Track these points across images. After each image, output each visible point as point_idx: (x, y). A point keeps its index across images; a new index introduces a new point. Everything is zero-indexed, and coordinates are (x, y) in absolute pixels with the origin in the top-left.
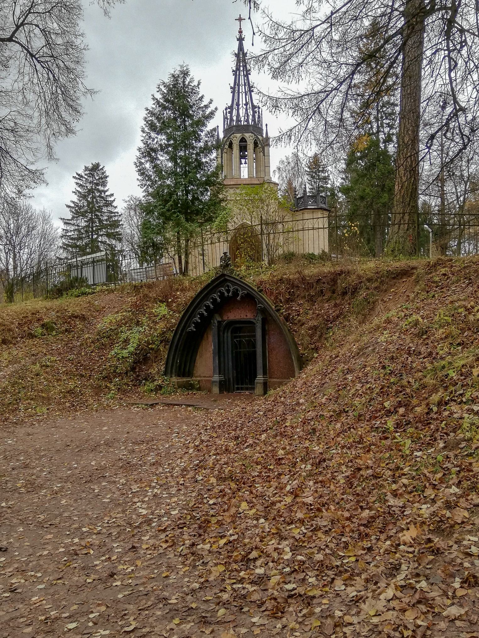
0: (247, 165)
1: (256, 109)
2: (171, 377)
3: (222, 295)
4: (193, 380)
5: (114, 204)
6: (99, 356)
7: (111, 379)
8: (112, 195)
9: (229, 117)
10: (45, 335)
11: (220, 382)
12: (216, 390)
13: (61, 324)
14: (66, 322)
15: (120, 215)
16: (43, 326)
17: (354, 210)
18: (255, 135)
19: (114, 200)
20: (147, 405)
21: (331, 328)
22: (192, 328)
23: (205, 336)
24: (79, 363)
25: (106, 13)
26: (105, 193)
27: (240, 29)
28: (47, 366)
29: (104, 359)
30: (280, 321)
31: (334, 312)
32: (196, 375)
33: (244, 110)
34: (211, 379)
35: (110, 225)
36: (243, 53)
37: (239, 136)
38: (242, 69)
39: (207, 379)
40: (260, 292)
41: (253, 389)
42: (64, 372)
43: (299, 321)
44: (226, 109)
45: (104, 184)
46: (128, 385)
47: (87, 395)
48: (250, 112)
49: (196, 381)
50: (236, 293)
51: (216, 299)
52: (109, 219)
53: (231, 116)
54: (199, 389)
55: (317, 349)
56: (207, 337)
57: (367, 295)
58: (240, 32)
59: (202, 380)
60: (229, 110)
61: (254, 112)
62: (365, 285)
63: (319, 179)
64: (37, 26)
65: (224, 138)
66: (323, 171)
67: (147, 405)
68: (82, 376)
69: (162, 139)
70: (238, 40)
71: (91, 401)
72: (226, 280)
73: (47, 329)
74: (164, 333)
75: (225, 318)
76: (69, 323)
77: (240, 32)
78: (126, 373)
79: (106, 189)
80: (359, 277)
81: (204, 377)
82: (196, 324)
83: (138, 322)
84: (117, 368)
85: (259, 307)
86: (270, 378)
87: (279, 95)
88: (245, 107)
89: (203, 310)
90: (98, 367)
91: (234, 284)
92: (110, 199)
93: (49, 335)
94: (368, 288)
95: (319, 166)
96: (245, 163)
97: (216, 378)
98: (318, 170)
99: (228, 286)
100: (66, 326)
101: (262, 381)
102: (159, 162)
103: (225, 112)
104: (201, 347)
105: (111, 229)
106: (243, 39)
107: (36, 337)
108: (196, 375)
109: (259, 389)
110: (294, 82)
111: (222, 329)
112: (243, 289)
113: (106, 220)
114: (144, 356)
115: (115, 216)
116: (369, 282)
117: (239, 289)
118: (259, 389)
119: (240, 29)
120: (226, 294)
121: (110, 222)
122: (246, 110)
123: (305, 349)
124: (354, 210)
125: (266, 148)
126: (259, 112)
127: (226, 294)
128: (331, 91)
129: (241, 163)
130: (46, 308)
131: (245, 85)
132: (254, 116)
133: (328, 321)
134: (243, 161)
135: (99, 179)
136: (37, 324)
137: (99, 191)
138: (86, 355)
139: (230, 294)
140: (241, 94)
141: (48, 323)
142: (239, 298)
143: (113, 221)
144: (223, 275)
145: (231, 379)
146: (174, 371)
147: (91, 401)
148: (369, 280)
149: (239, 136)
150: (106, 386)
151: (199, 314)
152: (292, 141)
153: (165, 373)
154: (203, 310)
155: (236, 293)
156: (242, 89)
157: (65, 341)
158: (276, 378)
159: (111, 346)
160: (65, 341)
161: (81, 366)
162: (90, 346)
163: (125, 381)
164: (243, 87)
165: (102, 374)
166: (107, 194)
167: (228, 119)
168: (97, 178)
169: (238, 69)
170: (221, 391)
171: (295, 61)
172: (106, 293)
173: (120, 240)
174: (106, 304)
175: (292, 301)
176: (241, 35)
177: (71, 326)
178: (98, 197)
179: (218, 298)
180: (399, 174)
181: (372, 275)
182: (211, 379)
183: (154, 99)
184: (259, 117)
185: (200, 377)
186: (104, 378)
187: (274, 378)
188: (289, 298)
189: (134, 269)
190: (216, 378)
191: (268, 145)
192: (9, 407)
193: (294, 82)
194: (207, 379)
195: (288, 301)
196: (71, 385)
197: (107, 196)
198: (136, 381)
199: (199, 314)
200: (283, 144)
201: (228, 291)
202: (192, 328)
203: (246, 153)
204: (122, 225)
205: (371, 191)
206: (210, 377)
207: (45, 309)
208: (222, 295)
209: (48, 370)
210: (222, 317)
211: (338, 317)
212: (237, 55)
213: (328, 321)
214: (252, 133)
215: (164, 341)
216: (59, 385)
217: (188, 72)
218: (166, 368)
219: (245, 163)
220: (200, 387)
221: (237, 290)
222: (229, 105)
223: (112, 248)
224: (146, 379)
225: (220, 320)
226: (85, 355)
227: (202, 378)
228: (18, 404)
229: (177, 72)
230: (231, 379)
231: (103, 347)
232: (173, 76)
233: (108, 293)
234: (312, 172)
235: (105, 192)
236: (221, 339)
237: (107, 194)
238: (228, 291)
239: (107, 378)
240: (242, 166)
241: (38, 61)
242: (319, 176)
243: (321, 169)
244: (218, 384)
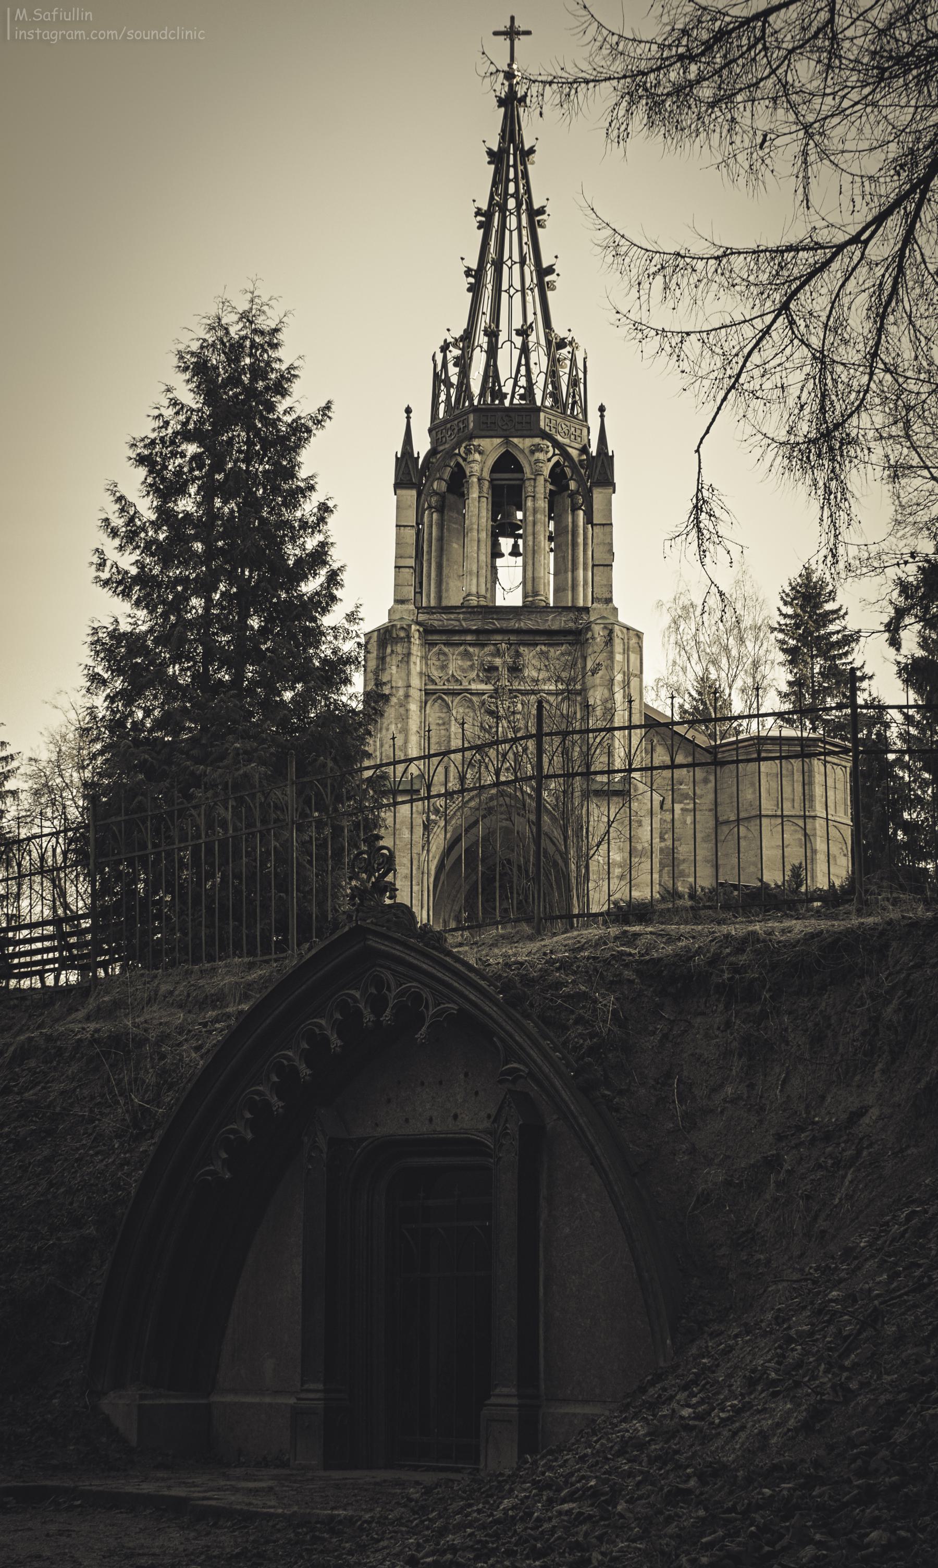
0: (520, 559)
1: (564, 352)
9: (454, 380)
33: (516, 353)
37: (492, 447)
38: (511, 203)
44: (445, 348)
48: (539, 360)
53: (464, 373)
60: (456, 352)
61: (554, 363)
65: (432, 453)
70: (501, 102)
88: (518, 341)
96: (515, 553)
103: (439, 358)
117: (426, 994)
120: (368, 1017)
122: (525, 350)
125: (598, 495)
126: (573, 361)
128: (840, 248)
129: (496, 553)
131: (523, 262)
132: (553, 374)
134: (506, 544)
140: (504, 296)
142: (421, 1034)
149: (492, 447)
156: (512, 276)
164: (516, 268)
167: (449, 385)
184: (574, 382)
191: (608, 482)
201: (378, 1003)
203: (520, 515)
212: (496, 157)
219: (515, 553)
222: (458, 332)
238: (378, 1003)
240: (499, 562)
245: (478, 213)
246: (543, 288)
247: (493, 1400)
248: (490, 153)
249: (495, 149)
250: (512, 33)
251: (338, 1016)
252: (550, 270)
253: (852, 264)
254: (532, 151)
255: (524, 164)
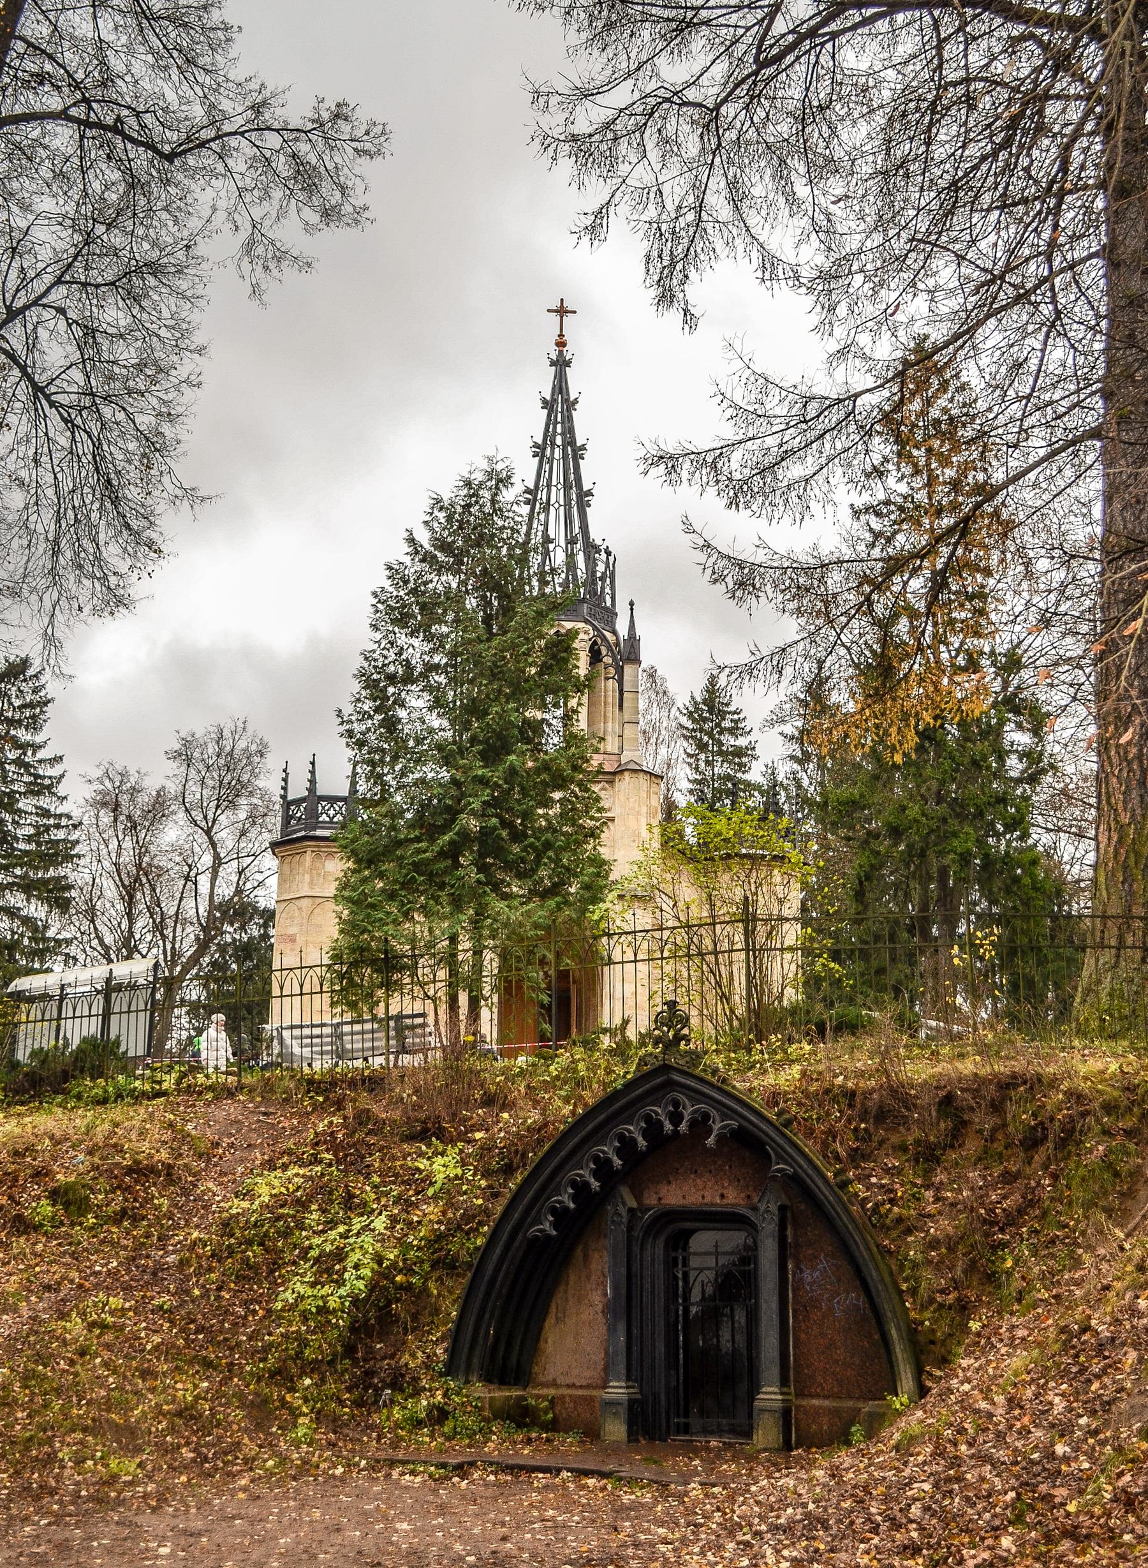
2: (467, 1382)
3: (653, 1128)
4: (536, 1396)
5: (61, 790)
6: (245, 1303)
7: (292, 1381)
8: (58, 759)
10: (62, 1224)
11: (632, 1403)
12: (616, 1430)
13: (107, 1193)
14: (119, 1187)
15: (75, 827)
16: (55, 1195)
17: (872, 866)
18: (595, 628)
19: (62, 776)
20: (443, 1466)
21: (1003, 1245)
22: (547, 1226)
23: (579, 1252)
24: (193, 1321)
25: (256, 291)
26: (34, 754)
27: (561, 335)
28: (104, 1326)
29: (261, 1313)
30: (853, 1220)
31: (1005, 1197)
32: (541, 1379)
34: (594, 1393)
35: (41, 856)
36: (566, 400)
38: (559, 440)
39: (580, 1392)
40: (786, 1126)
41: (748, 1433)
42: (156, 1348)
43: (900, 1220)
45: (34, 724)
46: (341, 1402)
47: (235, 1427)
49: (544, 1398)
50: (701, 1124)
51: (634, 1140)
52: (38, 834)
54: (553, 1426)
55: (964, 1308)
56: (586, 1257)
57: (1109, 1152)
58: (561, 344)
59: (563, 1397)
62: (1098, 1121)
63: (720, 753)
64: (61, 311)
66: (734, 731)
67: (443, 1466)
68: (207, 1364)
69: (416, 649)
71: (250, 1447)
72: (671, 1085)
73: (67, 1205)
74: (439, 1237)
75: (650, 1200)
76: (128, 1189)
77: (561, 344)
78: (331, 1363)
79: (39, 739)
80: (1076, 1096)
81: (568, 1386)
82: (560, 1215)
83: (351, 1196)
84: (304, 1343)
85: (778, 1171)
86: (800, 1394)
87: (760, 557)
89: (585, 1173)
90: (250, 1338)
91: (696, 1096)
92: (50, 772)
93: (73, 1224)
94: (1106, 1132)
95: (722, 715)
97: (618, 1390)
98: (718, 725)
99: (676, 1104)
100: (118, 1202)
101: (779, 1405)
102: (402, 713)
104: (562, 1288)
105: (37, 868)
106: (568, 364)
107: (37, 1228)
108: (541, 1379)
109: (766, 1434)
110: (787, 520)
111: (637, 1232)
112: (727, 1112)
113: (29, 839)
114: (381, 1309)
115: (58, 826)
116: (1109, 1114)
117: (713, 1113)
118: (766, 1434)
119: (561, 335)
120: (668, 1127)
121: (39, 844)
123: (924, 1308)
124: (872, 866)
127: (668, 1127)
130: (52, 1137)
133: (992, 1224)
135: (23, 707)
136: (36, 1190)
137: (17, 744)
138: (206, 1294)
139: (683, 1127)
141: (69, 1187)
142: (711, 1141)
143: (51, 841)
144: (665, 1068)
145: (663, 1397)
146: (476, 1360)
147: (250, 1447)
148: (1110, 1108)
150: (283, 1403)
151: (573, 1184)
152: (785, 682)
153: (450, 1369)
154: (585, 1173)
155: (701, 1124)
157: (125, 1248)
158: (818, 1396)
159: (272, 1272)
160: (125, 1248)
161: (197, 1332)
162: (210, 1270)
163: (331, 1387)
165: (264, 1360)
166: (40, 755)
168: (17, 703)
169: (548, 435)
170: (632, 1436)
171: (795, 470)
172: (209, 1096)
173: (63, 905)
174: (221, 1134)
175: (866, 1157)
176: (561, 352)
177: (135, 1200)
178: (13, 762)
179: (640, 1139)
180: (1108, 802)
181: (1116, 1093)
182: (594, 1393)
183: (411, 540)
185: (554, 1384)
186: (272, 1375)
187: (812, 1396)
188: (858, 1149)
189: (292, 1027)
190: (618, 1390)
192: (28, 1449)
193: (787, 520)
194: (580, 1392)
195: (856, 1157)
196: (184, 1390)
197: (40, 761)
198: (366, 1389)
199: (573, 1184)
200: (760, 685)
201: (676, 1118)
202: (547, 1226)
204: (79, 856)
205: (924, 814)
206: (588, 1387)
207: (47, 1141)
208: (653, 1128)
209: (109, 1337)
210: (638, 1197)
211: (1021, 1212)
212: (549, 405)
213: (992, 1224)
214: (586, 621)
215: (445, 1265)
216: (153, 1390)
217: (509, 477)
218: (452, 1352)
220: (555, 1420)
221: (706, 1117)
223: (36, 929)
224: (396, 1386)
225: (634, 1204)
226: (202, 1296)
227: (561, 1391)
228: (50, 1441)
229: (479, 477)
230: (663, 1397)
231: (247, 1274)
232: (468, 484)
233: (216, 1098)
234: (701, 730)
235: (36, 747)
236: (636, 1267)
237: (40, 755)
238: (676, 1118)
239: (282, 1376)
241: (52, 404)
242: (721, 744)
243: (727, 724)
244: (623, 1411)
245: (536, 445)
246: (583, 506)
247: (761, 1396)
248: (544, 401)
249: (548, 398)
250: (562, 311)
251: (643, 1125)
252: (589, 493)
253: (1039, 469)
254: (576, 401)
255: (569, 410)
